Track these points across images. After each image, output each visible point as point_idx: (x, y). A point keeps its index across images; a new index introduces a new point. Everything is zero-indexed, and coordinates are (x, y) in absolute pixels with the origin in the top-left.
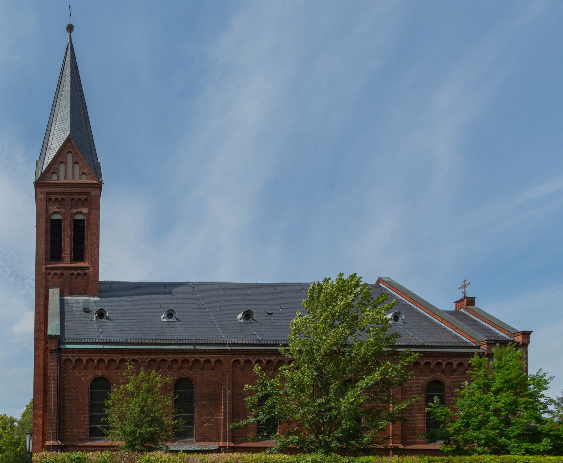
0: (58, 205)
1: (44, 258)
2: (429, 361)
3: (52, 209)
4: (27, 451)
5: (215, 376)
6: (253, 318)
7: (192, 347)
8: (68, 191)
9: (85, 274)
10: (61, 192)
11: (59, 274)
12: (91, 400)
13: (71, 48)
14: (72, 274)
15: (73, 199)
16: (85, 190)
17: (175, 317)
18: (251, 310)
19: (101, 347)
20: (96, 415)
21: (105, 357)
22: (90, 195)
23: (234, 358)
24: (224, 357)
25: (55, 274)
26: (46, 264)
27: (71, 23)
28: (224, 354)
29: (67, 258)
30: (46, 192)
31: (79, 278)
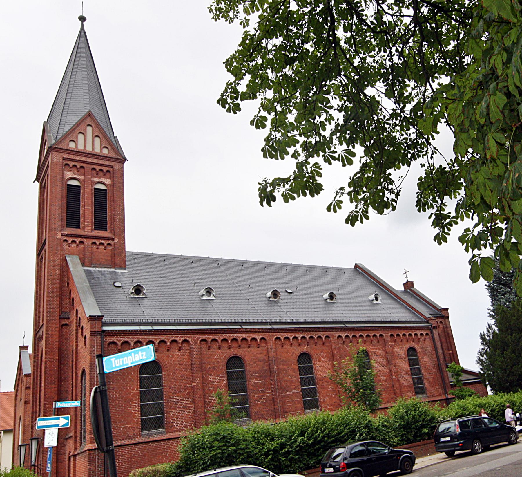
0: (76, 171)
1: (60, 224)
3: (68, 174)
4: (33, 463)
7: (239, 327)
9: (109, 244)
11: (78, 242)
12: (141, 388)
13: (82, 34)
15: (94, 169)
18: (277, 290)
19: (150, 328)
20: (147, 404)
21: (155, 339)
24: (267, 334)
25: (74, 242)
26: (61, 230)
27: (84, 15)
31: (102, 247)
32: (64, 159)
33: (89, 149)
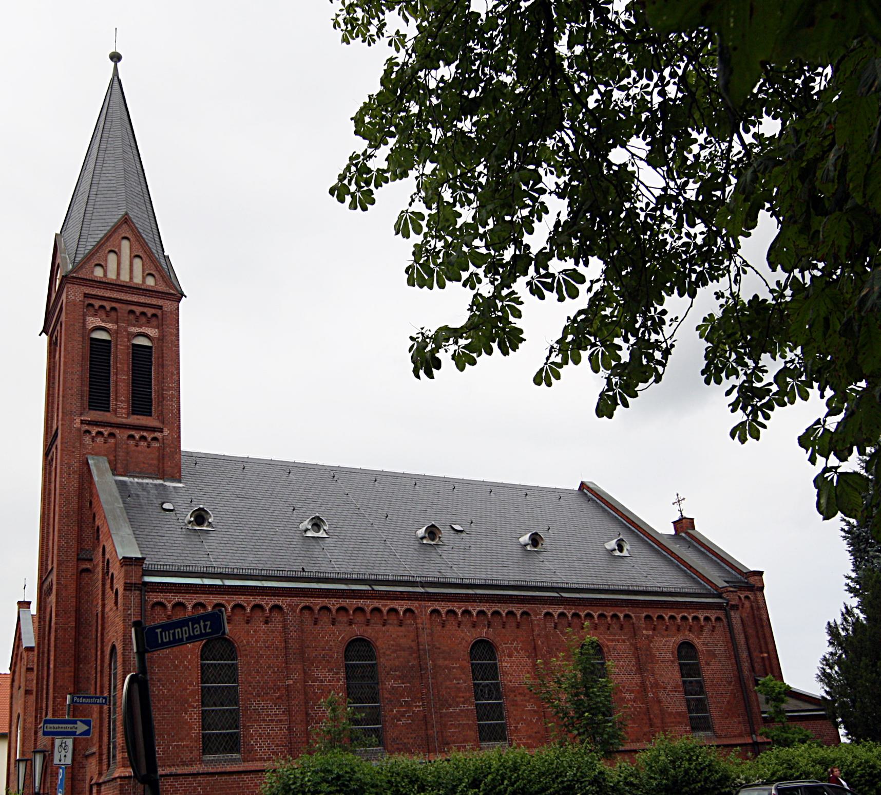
0: (104, 317)
2: (673, 614)
3: (93, 321)
5: (405, 636)
6: (440, 538)
8: (123, 298)
9: (155, 439)
10: (111, 298)
11: (106, 434)
13: (116, 81)
14: (131, 437)
15: (132, 312)
16: (154, 301)
17: (325, 530)
19: (218, 582)
20: (213, 710)
22: (161, 309)
23: (430, 606)
24: (416, 604)
25: (100, 434)
26: (81, 414)
27: (118, 51)
28: (416, 600)
29: (122, 408)
30: (85, 294)
32: (86, 296)
33: (125, 277)
